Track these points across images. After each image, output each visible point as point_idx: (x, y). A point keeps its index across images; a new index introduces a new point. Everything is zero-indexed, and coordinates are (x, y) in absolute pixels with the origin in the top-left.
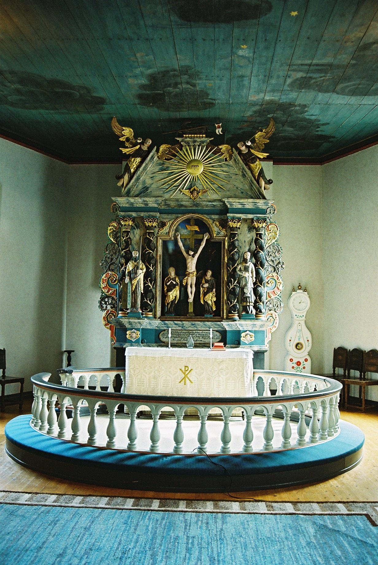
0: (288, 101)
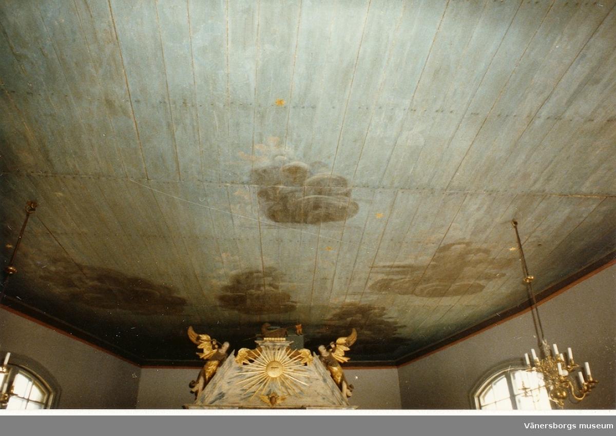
0: (368, 303)
